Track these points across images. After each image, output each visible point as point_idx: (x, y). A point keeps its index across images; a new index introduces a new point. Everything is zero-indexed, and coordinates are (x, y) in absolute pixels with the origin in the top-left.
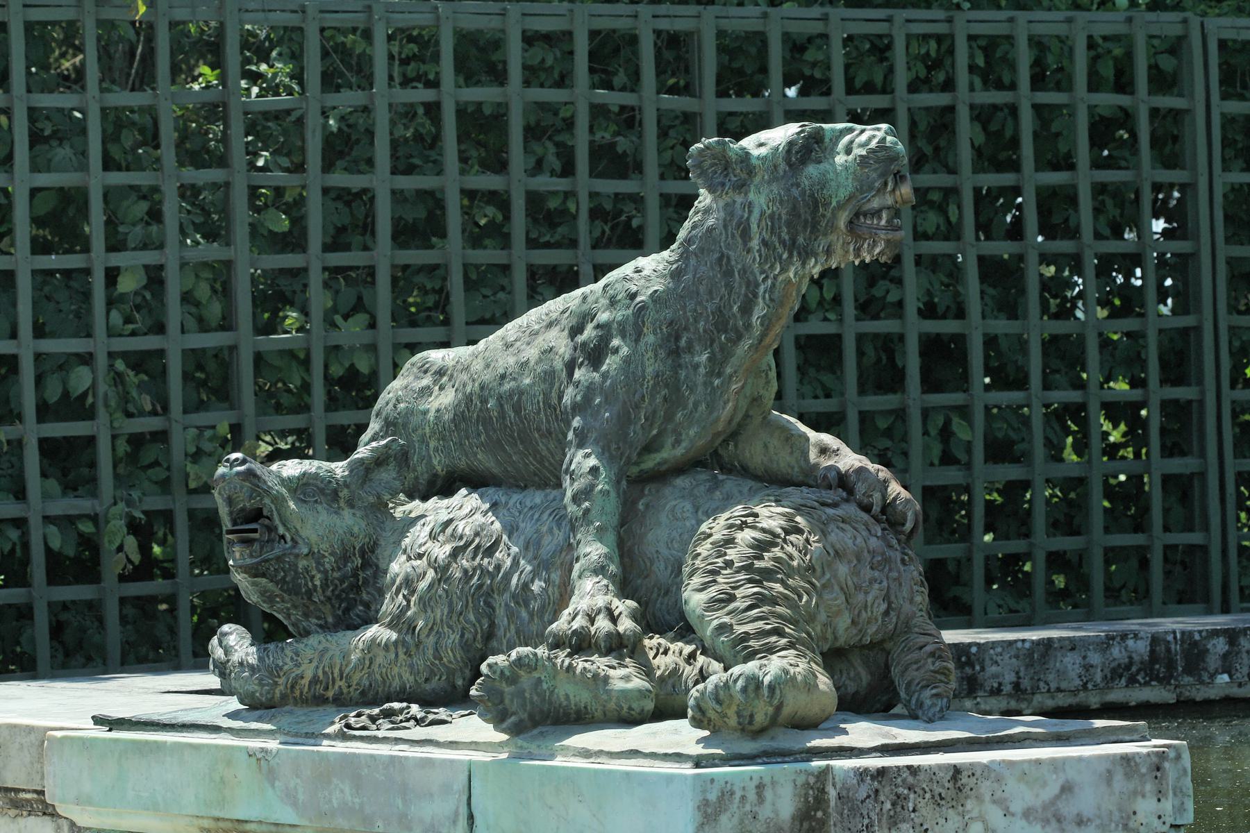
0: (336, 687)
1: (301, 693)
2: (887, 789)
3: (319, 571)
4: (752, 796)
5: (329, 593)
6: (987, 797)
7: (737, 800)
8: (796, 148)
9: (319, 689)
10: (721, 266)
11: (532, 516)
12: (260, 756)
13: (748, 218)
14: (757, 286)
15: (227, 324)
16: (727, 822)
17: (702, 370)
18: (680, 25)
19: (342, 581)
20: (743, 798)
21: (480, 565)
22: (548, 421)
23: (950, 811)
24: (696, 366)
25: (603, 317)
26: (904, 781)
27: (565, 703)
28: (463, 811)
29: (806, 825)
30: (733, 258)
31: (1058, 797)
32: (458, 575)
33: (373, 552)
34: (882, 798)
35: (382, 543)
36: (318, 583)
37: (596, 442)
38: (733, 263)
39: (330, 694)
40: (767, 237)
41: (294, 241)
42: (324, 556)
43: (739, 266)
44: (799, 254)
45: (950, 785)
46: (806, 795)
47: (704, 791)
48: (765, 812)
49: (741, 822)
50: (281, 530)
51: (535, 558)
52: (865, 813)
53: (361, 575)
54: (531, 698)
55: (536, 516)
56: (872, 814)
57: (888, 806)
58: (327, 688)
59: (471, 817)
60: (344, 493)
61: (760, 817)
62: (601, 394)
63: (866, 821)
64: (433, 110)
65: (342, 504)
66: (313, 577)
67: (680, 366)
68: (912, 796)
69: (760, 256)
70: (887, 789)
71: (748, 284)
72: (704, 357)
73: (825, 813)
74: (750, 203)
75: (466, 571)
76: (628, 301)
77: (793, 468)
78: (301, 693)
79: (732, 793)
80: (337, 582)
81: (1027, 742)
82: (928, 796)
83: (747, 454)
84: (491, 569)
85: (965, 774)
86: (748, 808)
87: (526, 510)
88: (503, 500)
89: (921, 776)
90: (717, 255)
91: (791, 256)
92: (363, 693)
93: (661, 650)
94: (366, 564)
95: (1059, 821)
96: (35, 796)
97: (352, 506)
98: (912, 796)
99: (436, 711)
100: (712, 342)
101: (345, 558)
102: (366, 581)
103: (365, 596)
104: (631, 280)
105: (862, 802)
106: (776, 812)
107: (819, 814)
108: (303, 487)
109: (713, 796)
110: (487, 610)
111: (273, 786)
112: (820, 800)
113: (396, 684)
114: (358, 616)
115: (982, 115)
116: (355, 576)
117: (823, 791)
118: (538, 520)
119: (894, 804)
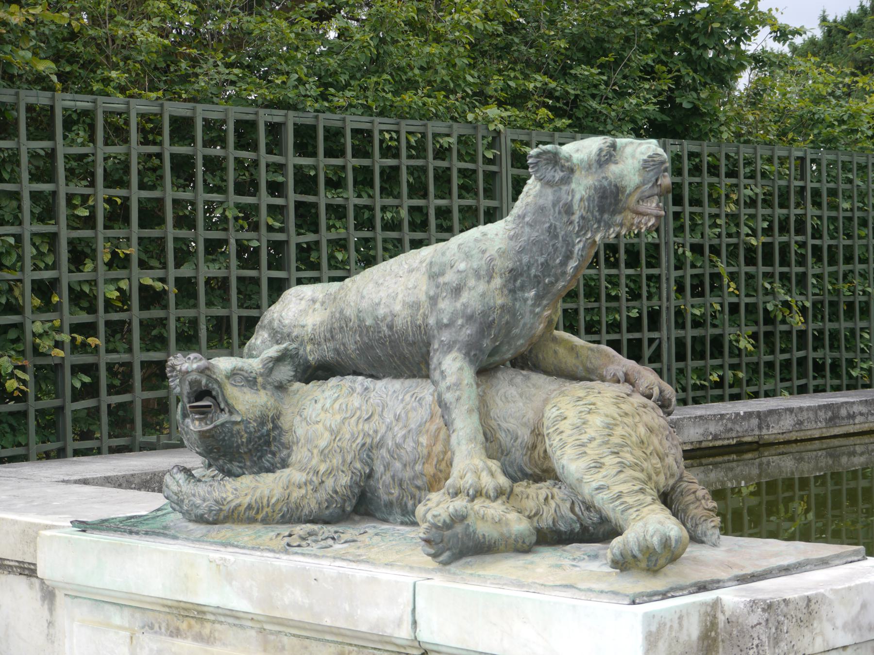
0: (264, 513)
1: (239, 516)
2: (773, 618)
3: (246, 432)
4: (676, 625)
5: (250, 447)
6: (824, 618)
7: (667, 630)
8: (604, 153)
9: (252, 513)
10: (550, 233)
11: (397, 397)
12: (219, 562)
13: (572, 200)
14: (574, 246)
15: (54, 266)
16: (662, 646)
17: (530, 302)
18: (277, 119)
19: (260, 438)
20: (671, 627)
21: (363, 430)
22: (414, 335)
23: (806, 630)
24: (525, 300)
25: (462, 266)
26: (781, 611)
27: (482, 540)
28: (408, 619)
29: (706, 643)
30: (558, 227)
31: (859, 612)
32: (348, 436)
33: (279, 419)
34: (770, 625)
35: (284, 412)
36: (244, 440)
37: (460, 350)
38: (558, 230)
39: (260, 517)
40: (584, 214)
41: (89, 222)
42: (250, 423)
43: (563, 233)
44: (605, 226)
45: (805, 611)
46: (706, 620)
47: (649, 625)
48: (683, 637)
49: (670, 646)
50: (222, 406)
51: (405, 427)
52: (755, 635)
53: (272, 434)
54: (462, 538)
55: (400, 397)
56: (761, 637)
57: (773, 630)
58: (257, 513)
59: (415, 623)
60: (260, 380)
61: (681, 640)
62: (462, 317)
63: (756, 642)
64: (159, 156)
65: (259, 387)
66: (242, 437)
67: (516, 299)
68: (786, 621)
69: (579, 226)
70: (773, 618)
71: (568, 245)
72: (533, 293)
73: (716, 633)
74: (573, 191)
75: (352, 435)
76: (480, 255)
77: (577, 368)
78: (239, 516)
79: (665, 625)
80: (257, 439)
81: (808, 567)
82: (794, 620)
83: (540, 356)
84: (371, 432)
85: (813, 601)
86: (674, 634)
87: (390, 393)
88: (372, 386)
89: (791, 606)
90: (547, 225)
91: (599, 227)
92: (283, 516)
93: (525, 496)
94: (276, 427)
95: (860, 630)
96: (17, 564)
97: (264, 388)
98: (786, 621)
99: (481, 573)
100: (539, 283)
101: (262, 423)
102: (274, 438)
103: (273, 448)
104: (481, 240)
105: (752, 627)
106: (689, 636)
107: (713, 634)
108: (233, 374)
109: (654, 628)
110: (368, 460)
111: (230, 584)
112: (714, 624)
113: (306, 511)
114: (268, 461)
115: (411, 170)
116: (268, 435)
117: (715, 617)
118: (402, 400)
119: (776, 629)
